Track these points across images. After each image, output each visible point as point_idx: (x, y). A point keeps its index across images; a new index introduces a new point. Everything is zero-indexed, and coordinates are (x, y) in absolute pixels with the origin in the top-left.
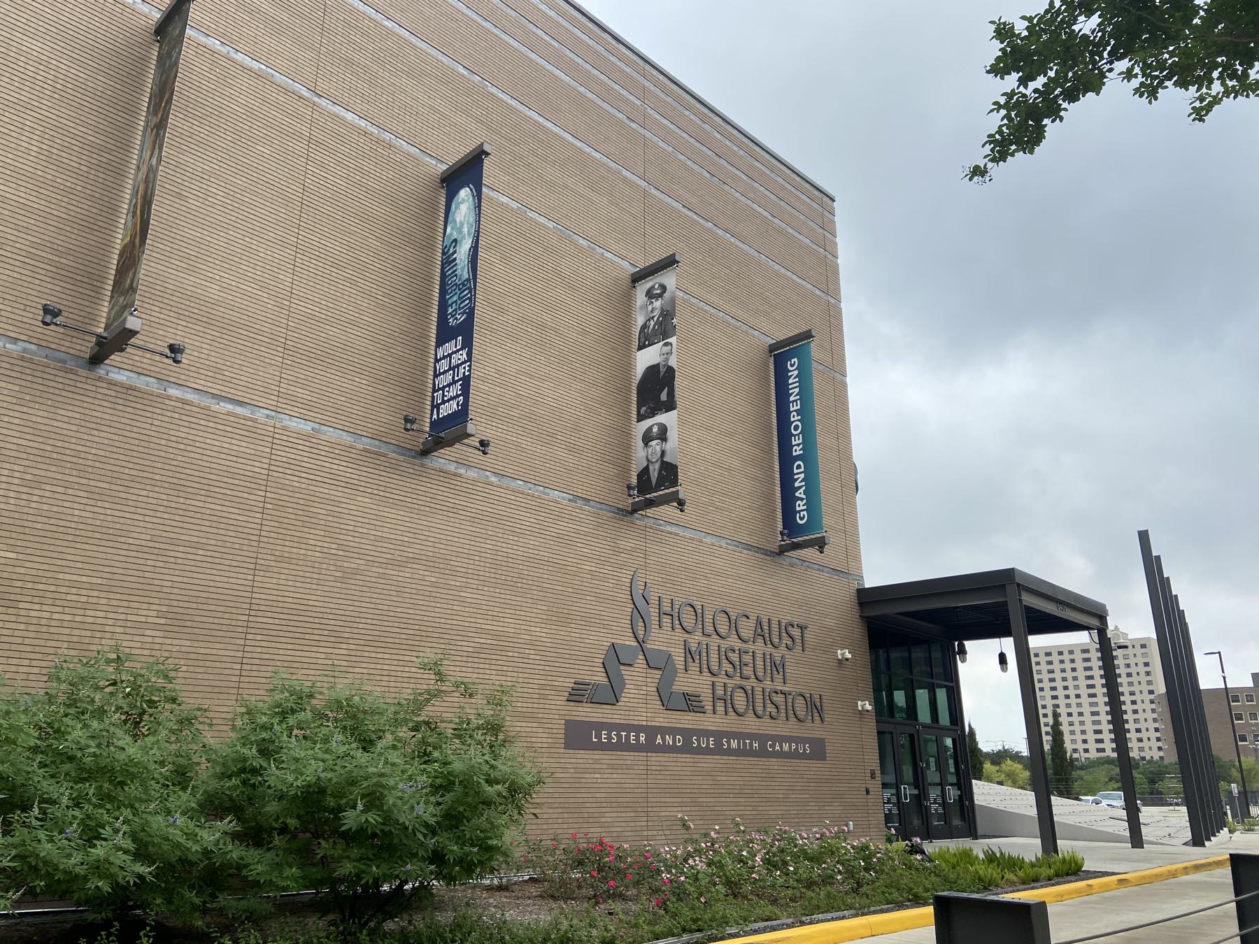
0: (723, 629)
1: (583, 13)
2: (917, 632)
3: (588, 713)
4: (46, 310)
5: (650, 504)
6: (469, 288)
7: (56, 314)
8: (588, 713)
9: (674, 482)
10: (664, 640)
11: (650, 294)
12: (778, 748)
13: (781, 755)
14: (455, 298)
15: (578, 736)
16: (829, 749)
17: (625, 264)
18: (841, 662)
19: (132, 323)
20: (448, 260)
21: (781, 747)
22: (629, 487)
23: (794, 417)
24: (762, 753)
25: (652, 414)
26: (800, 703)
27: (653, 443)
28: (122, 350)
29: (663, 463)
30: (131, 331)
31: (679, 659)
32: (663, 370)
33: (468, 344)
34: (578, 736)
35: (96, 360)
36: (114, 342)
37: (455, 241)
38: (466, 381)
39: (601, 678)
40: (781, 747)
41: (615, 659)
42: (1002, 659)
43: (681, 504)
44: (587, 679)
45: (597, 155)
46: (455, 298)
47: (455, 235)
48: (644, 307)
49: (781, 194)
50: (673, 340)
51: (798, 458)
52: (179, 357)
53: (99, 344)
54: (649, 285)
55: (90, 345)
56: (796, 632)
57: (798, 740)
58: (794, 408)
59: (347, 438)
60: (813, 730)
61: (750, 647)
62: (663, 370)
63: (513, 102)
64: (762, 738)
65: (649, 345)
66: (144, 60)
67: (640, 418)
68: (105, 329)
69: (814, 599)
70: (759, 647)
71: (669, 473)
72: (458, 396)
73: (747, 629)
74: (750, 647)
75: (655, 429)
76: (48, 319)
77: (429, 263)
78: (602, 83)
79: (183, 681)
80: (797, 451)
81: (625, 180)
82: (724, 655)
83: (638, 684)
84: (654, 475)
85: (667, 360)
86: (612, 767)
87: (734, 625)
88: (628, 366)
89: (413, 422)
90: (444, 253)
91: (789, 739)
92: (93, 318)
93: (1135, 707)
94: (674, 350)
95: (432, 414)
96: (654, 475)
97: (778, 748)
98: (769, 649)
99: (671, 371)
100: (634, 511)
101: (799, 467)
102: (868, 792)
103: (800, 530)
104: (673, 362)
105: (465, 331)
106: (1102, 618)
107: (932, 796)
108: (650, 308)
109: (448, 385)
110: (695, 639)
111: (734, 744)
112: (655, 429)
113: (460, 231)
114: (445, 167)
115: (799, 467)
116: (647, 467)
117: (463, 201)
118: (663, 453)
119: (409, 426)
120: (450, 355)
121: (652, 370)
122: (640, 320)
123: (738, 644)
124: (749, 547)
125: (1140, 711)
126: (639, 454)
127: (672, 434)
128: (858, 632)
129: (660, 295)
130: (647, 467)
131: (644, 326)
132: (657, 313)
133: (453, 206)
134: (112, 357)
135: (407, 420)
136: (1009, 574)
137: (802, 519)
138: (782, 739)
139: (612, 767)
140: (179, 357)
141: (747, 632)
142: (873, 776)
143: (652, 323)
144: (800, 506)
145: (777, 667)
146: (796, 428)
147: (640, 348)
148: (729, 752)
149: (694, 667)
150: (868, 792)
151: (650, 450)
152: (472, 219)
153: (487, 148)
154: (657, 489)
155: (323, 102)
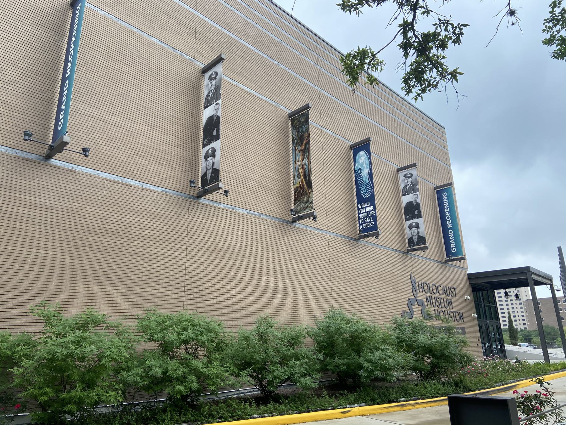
0: (435, 291)
1: (316, 35)
2: (484, 287)
4: (26, 134)
5: (301, 218)
6: (371, 187)
7: (30, 135)
9: (425, 243)
10: (421, 296)
11: (211, 79)
14: (364, 188)
17: (285, 110)
18: (466, 300)
19: (66, 138)
20: (358, 175)
22: (292, 211)
23: (447, 214)
25: (209, 143)
26: (457, 315)
27: (209, 159)
28: (61, 152)
29: (418, 236)
30: (65, 143)
31: (425, 302)
32: (215, 118)
33: (373, 204)
35: (49, 157)
36: (57, 147)
37: (360, 169)
38: (375, 218)
39: (407, 310)
41: (410, 303)
43: (315, 217)
45: (384, 128)
46: (364, 188)
47: (360, 167)
48: (208, 85)
49: (431, 130)
50: (220, 101)
51: (450, 229)
52: (87, 154)
53: (50, 149)
54: (405, 173)
55: (46, 150)
56: (453, 290)
59: (10, 151)
61: (442, 296)
62: (215, 118)
63: (362, 116)
65: (209, 106)
66: (287, 127)
67: (204, 146)
68: (52, 143)
69: (455, 278)
70: (444, 296)
71: (216, 173)
72: (371, 222)
73: (441, 290)
74: (442, 296)
75: (210, 151)
76: (27, 138)
77: (351, 176)
78: (382, 102)
79: (180, 308)
80: (449, 226)
81: (391, 136)
82: (436, 299)
83: (417, 310)
84: (209, 176)
85: (217, 112)
87: (437, 289)
88: (197, 116)
89: (194, 183)
90: (355, 173)
93: (513, 306)
94: (220, 107)
95: (360, 227)
96: (209, 176)
98: (447, 297)
99: (218, 118)
100: (408, 252)
101: (451, 232)
103: (454, 255)
104: (219, 114)
105: (371, 200)
106: (551, 280)
107: (494, 346)
108: (210, 86)
109: (366, 218)
110: (428, 295)
113: (362, 165)
114: (203, 66)
115: (451, 232)
116: (206, 172)
117: (362, 156)
118: (213, 163)
119: (192, 185)
120: (365, 208)
121: (210, 119)
122: (206, 93)
123: (439, 296)
124: (437, 261)
125: (515, 308)
126: (408, 233)
127: (218, 153)
128: (469, 289)
129: (410, 177)
130: (206, 172)
131: (208, 96)
132: (213, 88)
133: (357, 157)
134: (56, 155)
135: (191, 182)
136: (528, 268)
137: (454, 250)
140: (87, 154)
141: (441, 292)
143: (211, 93)
144: (453, 246)
145: (450, 303)
146: (448, 218)
147: (205, 108)
149: (429, 304)
151: (208, 163)
152: (367, 162)
153: (223, 56)
154: (417, 244)
155: (323, 129)
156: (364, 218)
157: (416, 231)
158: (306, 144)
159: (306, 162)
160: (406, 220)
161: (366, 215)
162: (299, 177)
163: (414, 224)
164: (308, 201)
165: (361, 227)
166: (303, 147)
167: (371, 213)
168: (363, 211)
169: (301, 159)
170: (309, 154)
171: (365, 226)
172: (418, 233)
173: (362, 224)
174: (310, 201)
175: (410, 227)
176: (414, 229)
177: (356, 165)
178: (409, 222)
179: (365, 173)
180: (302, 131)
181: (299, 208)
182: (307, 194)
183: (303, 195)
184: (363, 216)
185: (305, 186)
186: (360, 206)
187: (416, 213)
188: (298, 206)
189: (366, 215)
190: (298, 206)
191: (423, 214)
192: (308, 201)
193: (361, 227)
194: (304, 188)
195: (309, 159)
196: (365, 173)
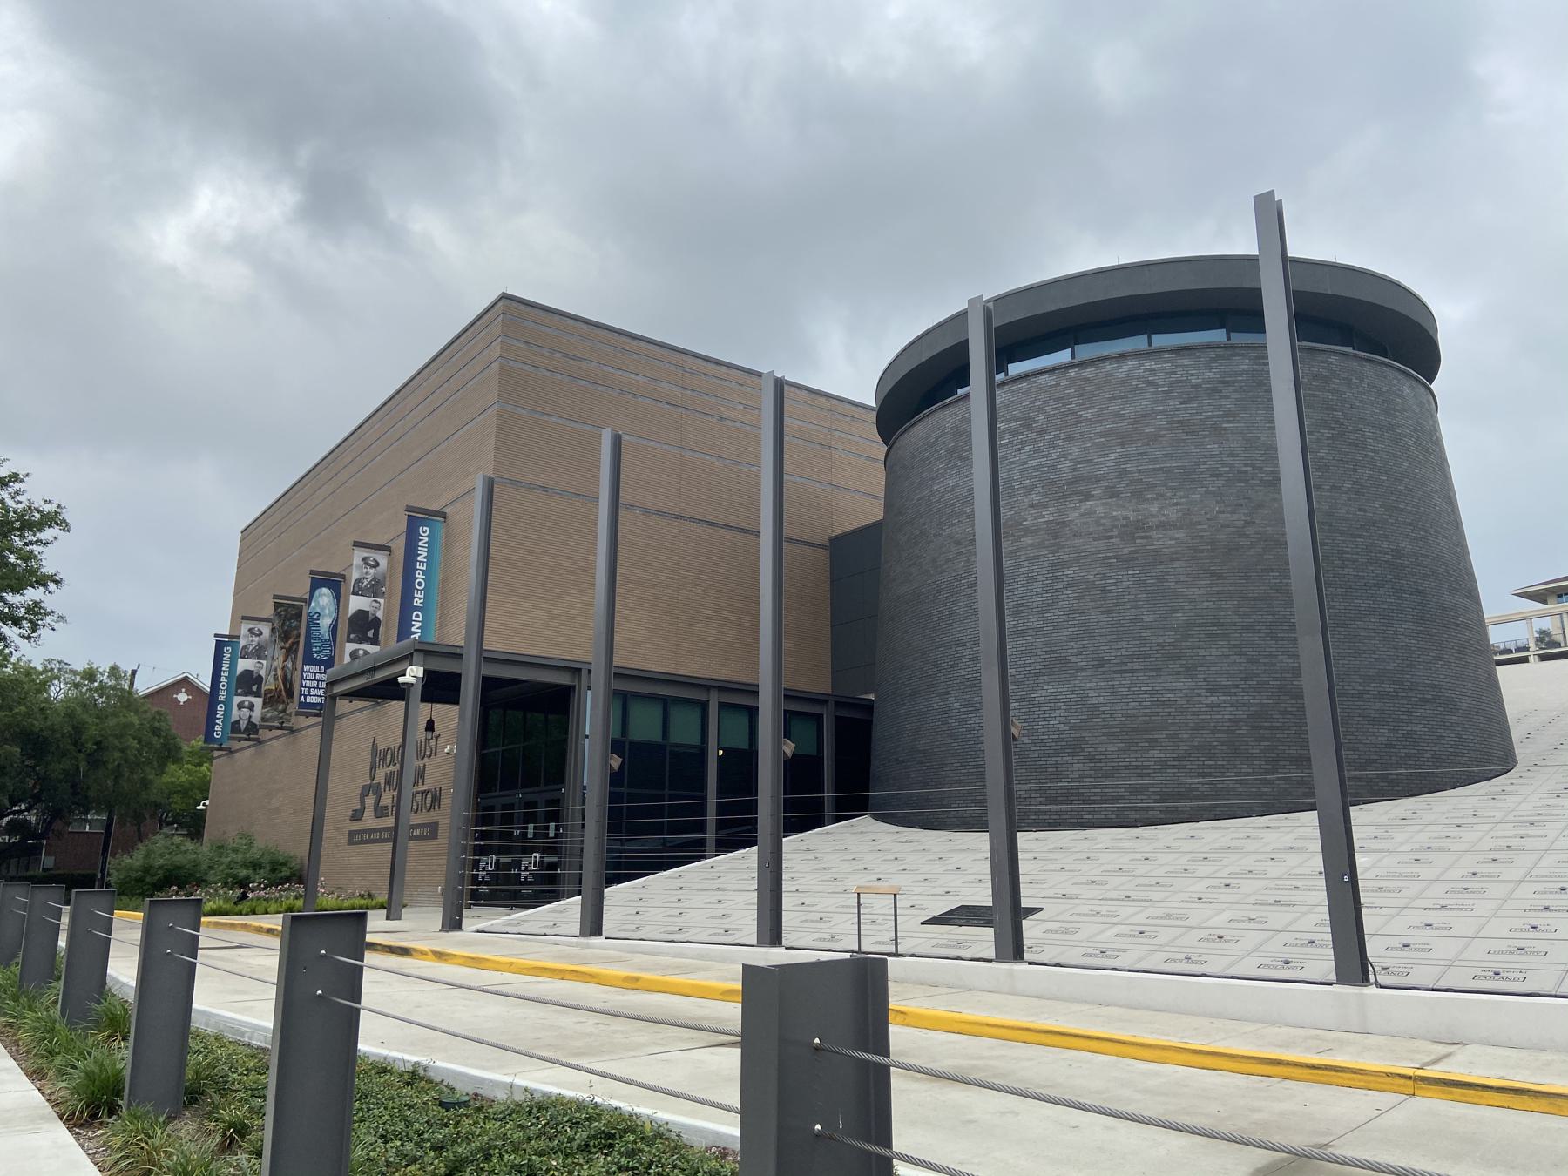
3: (357, 826)
80: (417, 603)
113: (323, 609)
144: (217, 728)
160: (350, 641)
164: (284, 711)
168: (311, 676)
171: (309, 700)
184: (308, 684)
186: (306, 668)
187: (370, 633)
191: (381, 637)
192: (284, 711)
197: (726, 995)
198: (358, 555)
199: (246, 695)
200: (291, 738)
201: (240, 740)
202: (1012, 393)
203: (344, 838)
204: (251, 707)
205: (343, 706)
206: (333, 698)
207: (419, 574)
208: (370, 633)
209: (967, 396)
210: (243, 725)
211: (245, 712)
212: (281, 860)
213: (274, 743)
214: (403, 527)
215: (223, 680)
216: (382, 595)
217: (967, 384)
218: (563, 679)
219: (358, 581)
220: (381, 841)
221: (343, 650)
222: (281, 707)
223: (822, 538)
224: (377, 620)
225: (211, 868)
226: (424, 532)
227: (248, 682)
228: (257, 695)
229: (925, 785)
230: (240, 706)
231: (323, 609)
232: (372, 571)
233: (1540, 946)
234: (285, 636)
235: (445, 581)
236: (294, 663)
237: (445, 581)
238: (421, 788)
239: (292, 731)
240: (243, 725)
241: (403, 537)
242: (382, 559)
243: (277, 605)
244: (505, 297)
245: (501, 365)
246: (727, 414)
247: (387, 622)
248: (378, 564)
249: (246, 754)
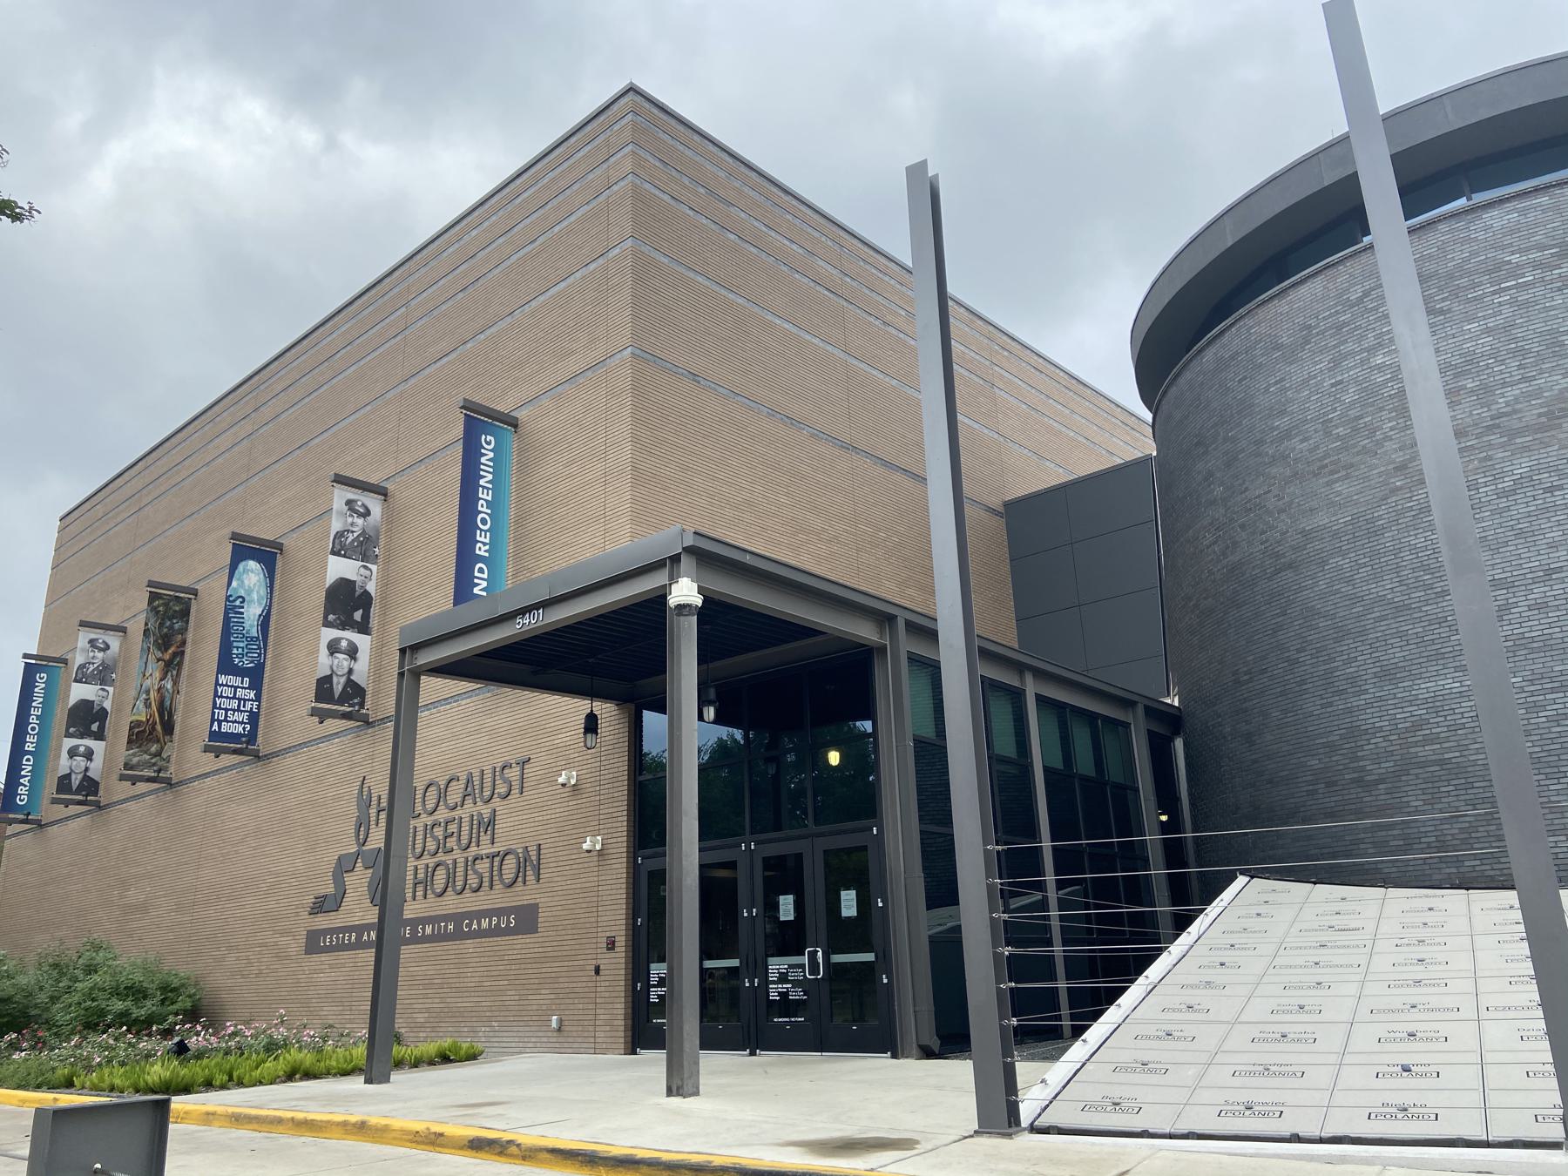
3: (323, 922)
8: (323, 922)
12: (475, 926)
13: (481, 934)
15: (314, 943)
16: (543, 915)
21: (479, 924)
24: (458, 935)
33: (256, 685)
34: (314, 943)
38: (254, 718)
40: (479, 924)
41: (343, 866)
42: (591, 724)
44: (323, 892)
47: (242, 593)
51: (29, 753)
57: (498, 912)
58: (485, 496)
60: (523, 895)
64: (457, 918)
86: (331, 966)
91: (488, 913)
92: (1442, 293)
97: (475, 926)
102: (597, 971)
111: (485, 924)
112: (82, 749)
113: (249, 591)
121: (85, 705)
130: (330, 677)
133: (241, 566)
138: (480, 915)
139: (331, 966)
142: (611, 945)
144: (22, 790)
148: (426, 939)
150: (597, 971)
152: (263, 592)
156: (226, 710)
157: (346, 664)
158: (175, 655)
159: (169, 686)
160: (327, 624)
161: (235, 704)
162: (147, 704)
163: (344, 644)
164: (158, 754)
165: (215, 727)
166: (167, 657)
167: (248, 705)
168: (228, 692)
169: (157, 675)
170: (178, 675)
171: (225, 728)
172: (350, 671)
173: (220, 722)
174: (164, 755)
175: (333, 648)
176: (341, 656)
177: (234, 584)
178: (334, 633)
179: (252, 612)
180: (171, 627)
181: (135, 760)
182: (158, 741)
183: (149, 740)
184: (225, 703)
185: (159, 727)
186: (223, 679)
187: (358, 615)
188: (134, 755)
189: (235, 704)
190: (134, 755)
191: (374, 622)
192: (158, 754)
193: (215, 727)
194: (154, 728)
195: (175, 682)
196: (252, 612)
197: (185, 1117)
198: (84, 637)
199: (343, 626)
200: (169, 796)
201: (67, 803)
202: (1523, 212)
203: (296, 944)
204: (352, 652)
205: (432, 687)
206: (417, 674)
207: (482, 506)
208: (358, 615)
209: (1371, 247)
210: (76, 781)
211: (80, 762)
212: (176, 983)
213: (132, 805)
214: (458, 430)
215: (33, 720)
216: (112, 683)
217: (1367, 232)
218: (865, 631)
219: (82, 667)
220: (359, 945)
221: (60, 747)
222: (154, 749)
223: (996, 502)
224: (366, 594)
225: (54, 999)
226: (488, 442)
227: (87, 719)
228: (364, 628)
229: (1332, 816)
230: (73, 753)
231: (249, 591)
232: (100, 655)
233: (1189, 1031)
234: (164, 642)
235: (520, 521)
236: (175, 682)
237: (520, 521)
238: (486, 849)
239: (40, 825)
240: (338, 685)
241: (459, 447)
242: (114, 642)
243: (153, 597)
244: (632, 89)
245: (634, 184)
246: (889, 318)
247: (384, 598)
248: (108, 647)
249: (72, 830)
